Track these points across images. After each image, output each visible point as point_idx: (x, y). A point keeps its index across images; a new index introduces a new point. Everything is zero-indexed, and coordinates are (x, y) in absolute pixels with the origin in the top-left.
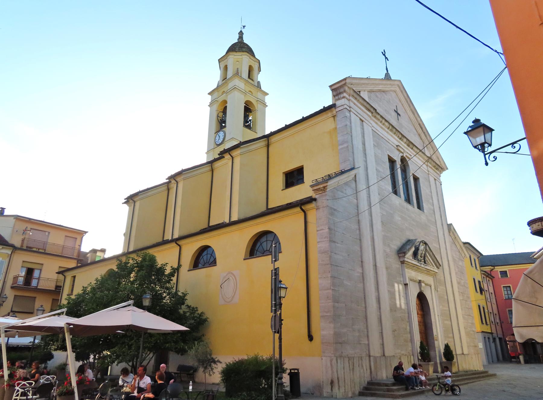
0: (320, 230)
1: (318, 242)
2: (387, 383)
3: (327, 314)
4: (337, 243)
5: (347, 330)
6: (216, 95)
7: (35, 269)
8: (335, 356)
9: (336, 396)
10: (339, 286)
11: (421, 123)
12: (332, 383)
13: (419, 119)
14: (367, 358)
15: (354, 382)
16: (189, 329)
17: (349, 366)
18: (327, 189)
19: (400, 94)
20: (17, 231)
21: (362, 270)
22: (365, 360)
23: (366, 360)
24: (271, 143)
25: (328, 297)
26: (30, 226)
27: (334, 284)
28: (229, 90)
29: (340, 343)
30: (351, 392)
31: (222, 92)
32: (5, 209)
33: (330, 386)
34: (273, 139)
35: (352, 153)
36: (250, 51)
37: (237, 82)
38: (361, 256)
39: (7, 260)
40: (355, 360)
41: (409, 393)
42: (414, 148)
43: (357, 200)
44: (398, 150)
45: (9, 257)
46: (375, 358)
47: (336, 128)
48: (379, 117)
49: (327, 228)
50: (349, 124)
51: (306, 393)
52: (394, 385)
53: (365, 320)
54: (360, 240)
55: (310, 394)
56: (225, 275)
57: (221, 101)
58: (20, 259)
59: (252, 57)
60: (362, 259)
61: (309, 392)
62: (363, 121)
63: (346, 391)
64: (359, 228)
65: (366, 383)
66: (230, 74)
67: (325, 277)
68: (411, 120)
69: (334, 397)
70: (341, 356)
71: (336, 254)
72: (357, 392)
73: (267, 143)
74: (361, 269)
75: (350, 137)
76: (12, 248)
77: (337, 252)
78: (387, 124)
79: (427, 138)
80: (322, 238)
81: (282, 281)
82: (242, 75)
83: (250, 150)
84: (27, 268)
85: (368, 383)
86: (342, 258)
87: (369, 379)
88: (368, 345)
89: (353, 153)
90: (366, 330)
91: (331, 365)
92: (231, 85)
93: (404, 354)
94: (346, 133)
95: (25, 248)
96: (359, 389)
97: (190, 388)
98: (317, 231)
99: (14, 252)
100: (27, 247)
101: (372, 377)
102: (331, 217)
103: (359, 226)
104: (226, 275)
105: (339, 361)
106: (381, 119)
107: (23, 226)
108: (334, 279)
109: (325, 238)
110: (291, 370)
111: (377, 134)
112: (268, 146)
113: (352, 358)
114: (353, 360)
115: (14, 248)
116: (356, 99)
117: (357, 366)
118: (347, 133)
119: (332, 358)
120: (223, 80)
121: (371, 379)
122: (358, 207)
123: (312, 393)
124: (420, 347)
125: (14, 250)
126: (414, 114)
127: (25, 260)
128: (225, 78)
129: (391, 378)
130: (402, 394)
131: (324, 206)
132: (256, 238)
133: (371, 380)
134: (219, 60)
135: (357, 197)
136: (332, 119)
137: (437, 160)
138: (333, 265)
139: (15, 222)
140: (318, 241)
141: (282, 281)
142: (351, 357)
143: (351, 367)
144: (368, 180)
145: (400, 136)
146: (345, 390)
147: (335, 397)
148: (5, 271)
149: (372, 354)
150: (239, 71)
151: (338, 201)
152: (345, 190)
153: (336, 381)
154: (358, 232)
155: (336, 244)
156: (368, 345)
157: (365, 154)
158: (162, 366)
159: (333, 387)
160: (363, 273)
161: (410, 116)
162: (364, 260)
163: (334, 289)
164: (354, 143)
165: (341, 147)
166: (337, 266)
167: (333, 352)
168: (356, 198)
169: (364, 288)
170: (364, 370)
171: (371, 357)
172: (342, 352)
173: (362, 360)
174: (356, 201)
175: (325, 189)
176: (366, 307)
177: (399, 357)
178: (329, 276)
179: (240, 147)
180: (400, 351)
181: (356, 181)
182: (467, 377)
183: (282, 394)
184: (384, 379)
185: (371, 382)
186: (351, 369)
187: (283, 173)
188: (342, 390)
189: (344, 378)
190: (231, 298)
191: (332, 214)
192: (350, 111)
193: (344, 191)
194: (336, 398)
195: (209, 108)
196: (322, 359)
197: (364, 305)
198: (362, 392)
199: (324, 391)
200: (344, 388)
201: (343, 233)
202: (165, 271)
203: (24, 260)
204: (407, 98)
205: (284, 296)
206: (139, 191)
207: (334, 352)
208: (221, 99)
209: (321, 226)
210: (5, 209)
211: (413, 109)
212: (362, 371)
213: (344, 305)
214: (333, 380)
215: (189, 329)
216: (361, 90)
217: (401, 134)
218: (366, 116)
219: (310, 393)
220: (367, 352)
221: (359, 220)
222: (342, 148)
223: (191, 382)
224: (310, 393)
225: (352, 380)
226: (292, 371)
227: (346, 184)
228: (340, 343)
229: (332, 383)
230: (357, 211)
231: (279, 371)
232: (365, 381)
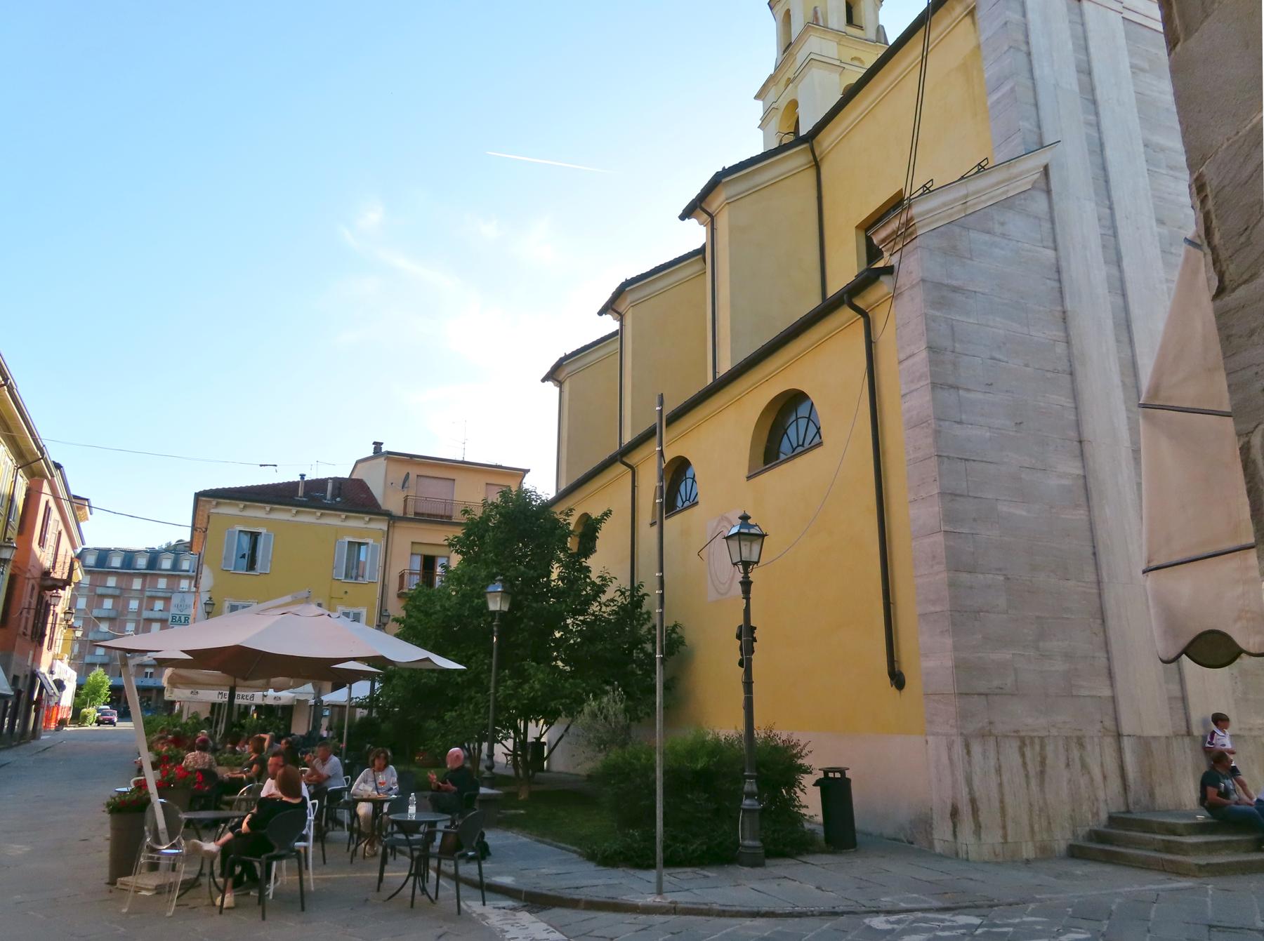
0: (907, 359)
1: (902, 396)
2: (1170, 824)
3: (933, 609)
4: (968, 390)
5: (1013, 654)
6: (772, 94)
7: (438, 556)
8: (961, 734)
10: (975, 520)
12: (955, 813)
14: (1109, 741)
15: (1048, 817)
16: (191, 658)
17: (1025, 764)
18: (915, 230)
20: (392, 484)
21: (1084, 467)
22: (1097, 749)
24: (824, 154)
25: (934, 557)
26: (414, 471)
27: (949, 517)
28: (798, 73)
29: (980, 694)
30: (1030, 844)
31: (784, 83)
32: (382, 444)
33: (950, 824)
34: (827, 140)
35: (1033, 109)
37: (816, 44)
38: (1078, 425)
39: (383, 543)
40: (1050, 749)
41: (1251, 862)
43: (1056, 249)
45: (386, 536)
46: (1145, 744)
47: (978, 47)
49: (924, 347)
50: (1015, 17)
51: (895, 839)
52: (1201, 829)
53: (1099, 621)
54: (1071, 374)
55: (903, 842)
56: (715, 524)
57: (786, 104)
58: (405, 537)
60: (1080, 434)
61: (902, 836)
63: (1010, 839)
64: (1068, 336)
65: (1104, 816)
66: (797, 27)
67: (924, 496)
69: (961, 856)
70: (983, 735)
71: (960, 423)
72: (1061, 846)
73: (812, 157)
74: (1079, 464)
75: (1022, 58)
76: (386, 518)
77: (964, 417)
80: (912, 382)
81: (750, 518)
82: (829, 22)
83: (758, 186)
84: (421, 555)
85: (1113, 820)
86: (988, 434)
87: (1117, 806)
88: (1114, 699)
89: (1036, 105)
90: (1101, 655)
91: (950, 759)
92: (801, 56)
94: (1006, 48)
95: (413, 516)
96: (1069, 835)
97: (410, 811)
98: (900, 362)
99: (394, 527)
100: (416, 514)
101: (1131, 800)
102: (938, 314)
103: (1066, 329)
104: (717, 526)
105: (976, 748)
107: (401, 473)
108: (953, 500)
109: (920, 378)
110: (826, 772)
112: (817, 165)
113: (1037, 741)
114: (1042, 747)
115: (391, 518)
117: (1062, 765)
118: (1011, 47)
119: (953, 738)
120: (784, 52)
121: (1127, 806)
122: (1059, 272)
123: (911, 840)
125: (391, 522)
127: (416, 541)
128: (787, 47)
129: (820, 824)
130: (1208, 865)
131: (914, 282)
132: (770, 422)
133: (1128, 811)
134: (771, 4)
135: (1055, 241)
136: (968, 20)
138: (948, 457)
139: (387, 465)
140: (903, 392)
141: (750, 518)
142: (1032, 738)
143: (1033, 769)
144: (1107, 182)
146: (1005, 836)
147: (965, 856)
148: (382, 564)
149: (1126, 729)
150: (819, 15)
151: (969, 262)
152: (1003, 224)
153: (965, 809)
154: (1060, 349)
155: (961, 392)
156: (1114, 702)
157: (1094, 102)
158: (453, 753)
159: (958, 825)
160: (1085, 477)
162: (1087, 435)
163: (952, 530)
164: (1037, 73)
165: (995, 97)
166: (966, 460)
167: (952, 722)
168: (1051, 244)
169: (1091, 524)
170: (1092, 780)
171: (1125, 739)
172: (991, 723)
173: (1081, 745)
174: (1051, 253)
175: (910, 230)
176: (1099, 582)
178: (936, 491)
179: (720, 181)
181: (1048, 192)
183: (754, 839)
184: (1188, 808)
185: (1128, 816)
186: (1032, 772)
187: (856, 227)
188: (992, 837)
189: (1002, 802)
190: (729, 582)
191: (940, 303)
193: (998, 229)
194: (967, 860)
195: (761, 132)
196: (927, 742)
197: (1091, 577)
198: (1080, 848)
199: (935, 836)
200: (1000, 832)
201: (993, 358)
202: (599, 531)
203: (413, 541)
205: (756, 560)
206: (563, 355)
207: (957, 721)
208: (783, 103)
209: (909, 345)
210: (382, 444)
212: (1083, 781)
213: (1002, 578)
214: (957, 806)
215: (191, 658)
219: (905, 840)
220: (1109, 723)
221: (1064, 312)
222: (998, 102)
223: (413, 794)
224: (905, 840)
225: (1036, 808)
226: (831, 775)
227: (1007, 204)
228: (980, 694)
229: (955, 813)
230: (1056, 285)
231: (746, 773)
232: (1096, 814)
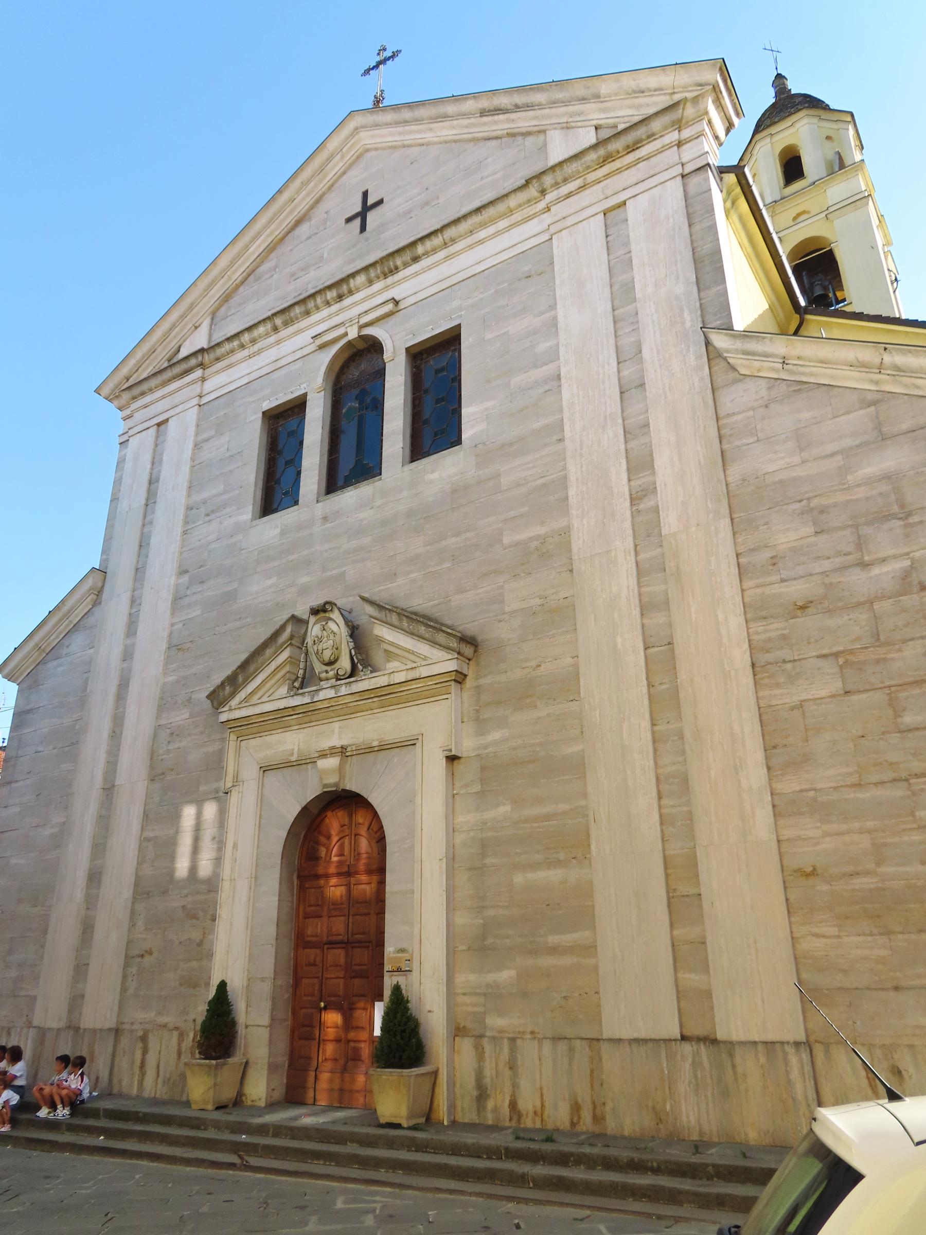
23: (20, 1036)
36: (812, 103)
42: (420, 249)
48: (227, 347)
59: (824, 114)
78: (261, 329)
93: (171, 1026)
106: (236, 343)
111: (225, 398)
116: (143, 394)
124: (408, 1001)
137: (639, 107)
161: (443, 139)
177: (140, 1033)
180: (153, 1014)
182: (453, 1161)
217: (330, 287)
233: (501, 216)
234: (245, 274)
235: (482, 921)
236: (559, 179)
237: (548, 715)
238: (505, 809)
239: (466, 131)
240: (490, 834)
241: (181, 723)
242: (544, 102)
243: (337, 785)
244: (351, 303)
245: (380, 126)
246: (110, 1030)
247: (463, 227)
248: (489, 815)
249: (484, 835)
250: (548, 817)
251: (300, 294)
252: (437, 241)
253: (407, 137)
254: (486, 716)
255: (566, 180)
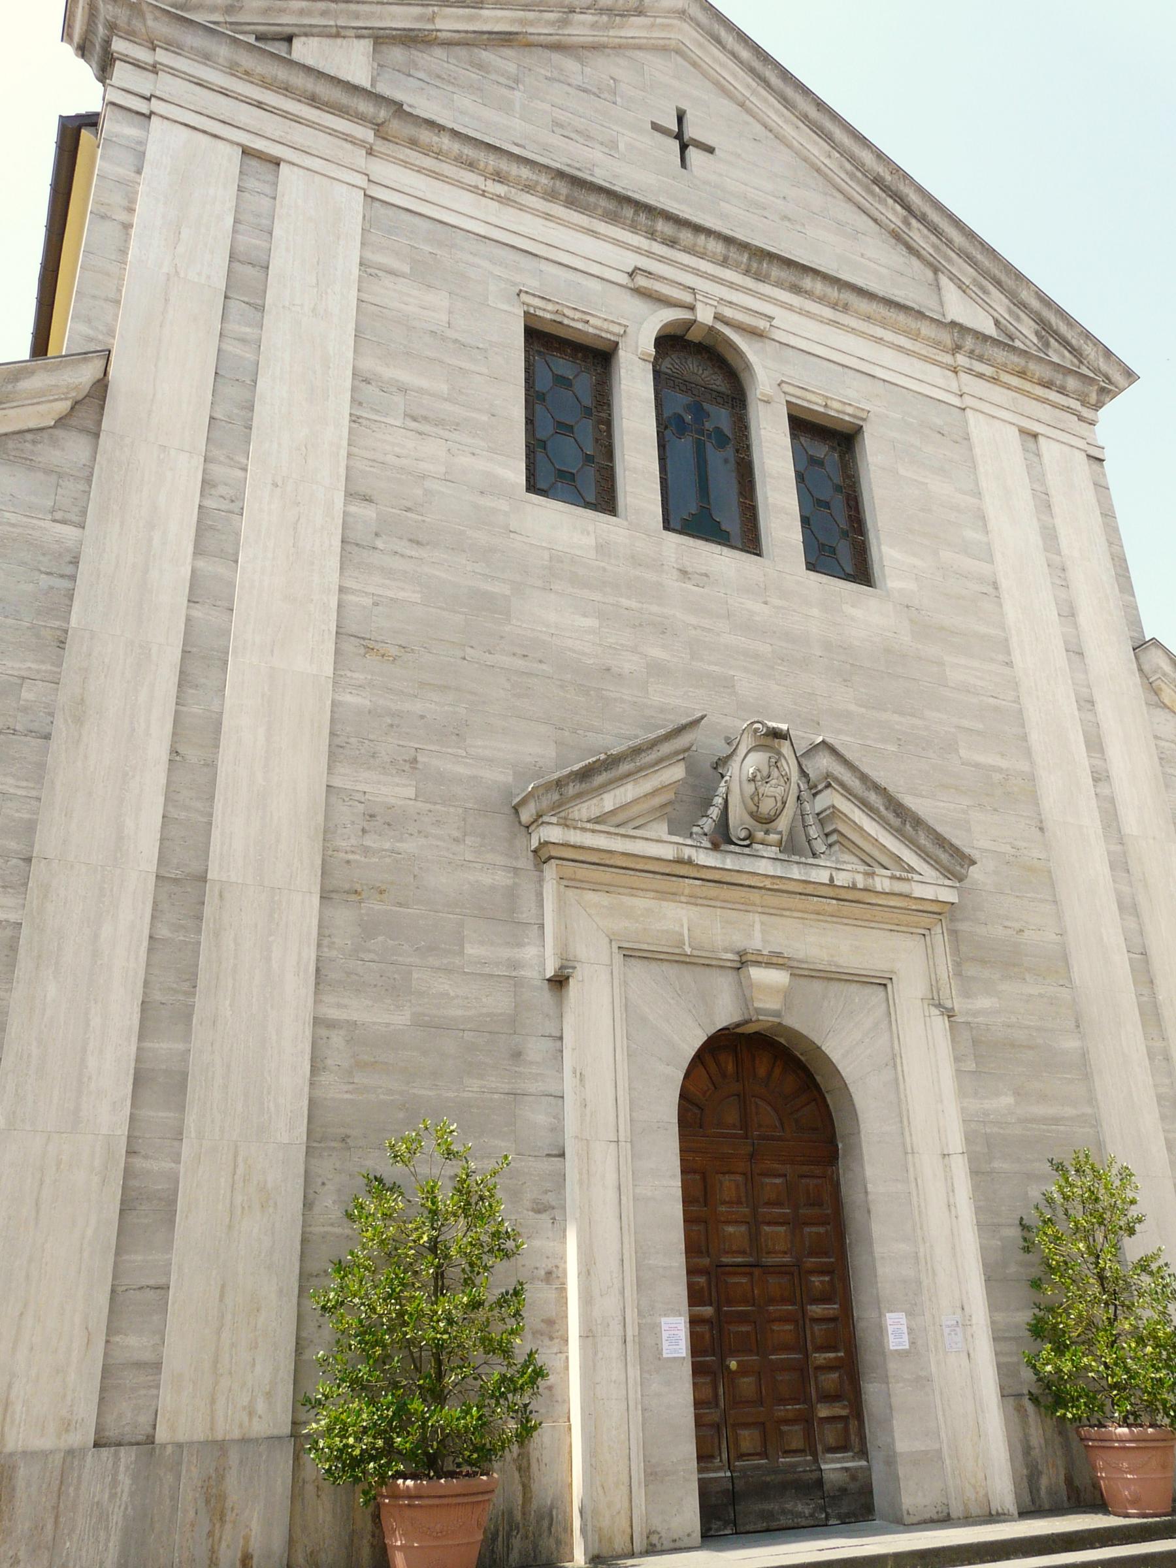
9: (1144, 874)
11: (881, 170)
13: (867, 158)
19: (712, 56)
44: (640, 292)
62: (1035, 436)
68: (818, 170)
79: (949, 243)
126: (828, 138)
145: (611, 205)
192: (964, 409)
204: (757, 65)
211: (813, 113)
216: (295, 30)
218: (272, 125)
233: (906, 333)
234: (456, 36)
235: (999, 1243)
236: (977, 352)
237: (1041, 995)
238: (1007, 1100)
239: (843, 176)
240: (995, 1130)
241: (393, 801)
242: (956, 245)
243: (777, 1014)
244: (685, 262)
245: (724, 47)
246: (273, 1440)
247: (863, 305)
248: (991, 1104)
249: (988, 1131)
250: (1056, 1120)
251: (579, 169)
252: (833, 293)
253: (753, 99)
254: (969, 974)
255: (980, 359)
